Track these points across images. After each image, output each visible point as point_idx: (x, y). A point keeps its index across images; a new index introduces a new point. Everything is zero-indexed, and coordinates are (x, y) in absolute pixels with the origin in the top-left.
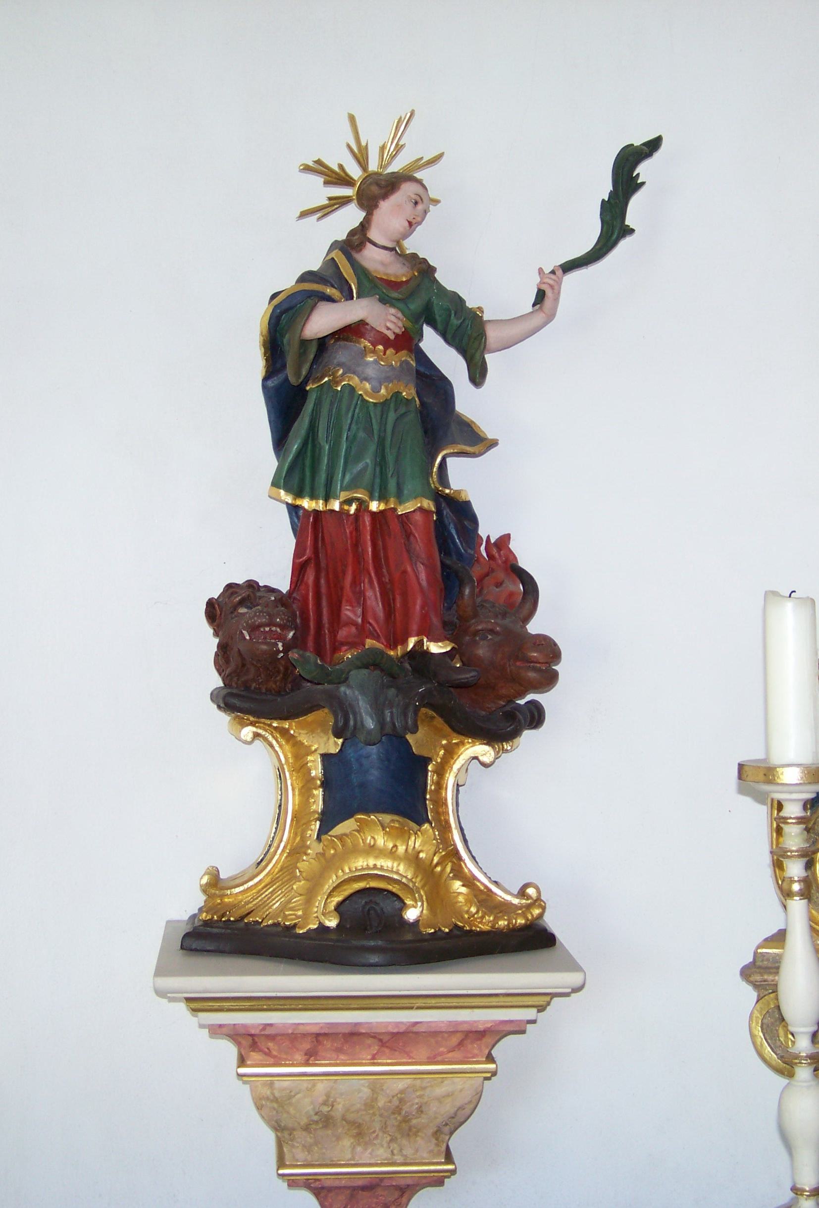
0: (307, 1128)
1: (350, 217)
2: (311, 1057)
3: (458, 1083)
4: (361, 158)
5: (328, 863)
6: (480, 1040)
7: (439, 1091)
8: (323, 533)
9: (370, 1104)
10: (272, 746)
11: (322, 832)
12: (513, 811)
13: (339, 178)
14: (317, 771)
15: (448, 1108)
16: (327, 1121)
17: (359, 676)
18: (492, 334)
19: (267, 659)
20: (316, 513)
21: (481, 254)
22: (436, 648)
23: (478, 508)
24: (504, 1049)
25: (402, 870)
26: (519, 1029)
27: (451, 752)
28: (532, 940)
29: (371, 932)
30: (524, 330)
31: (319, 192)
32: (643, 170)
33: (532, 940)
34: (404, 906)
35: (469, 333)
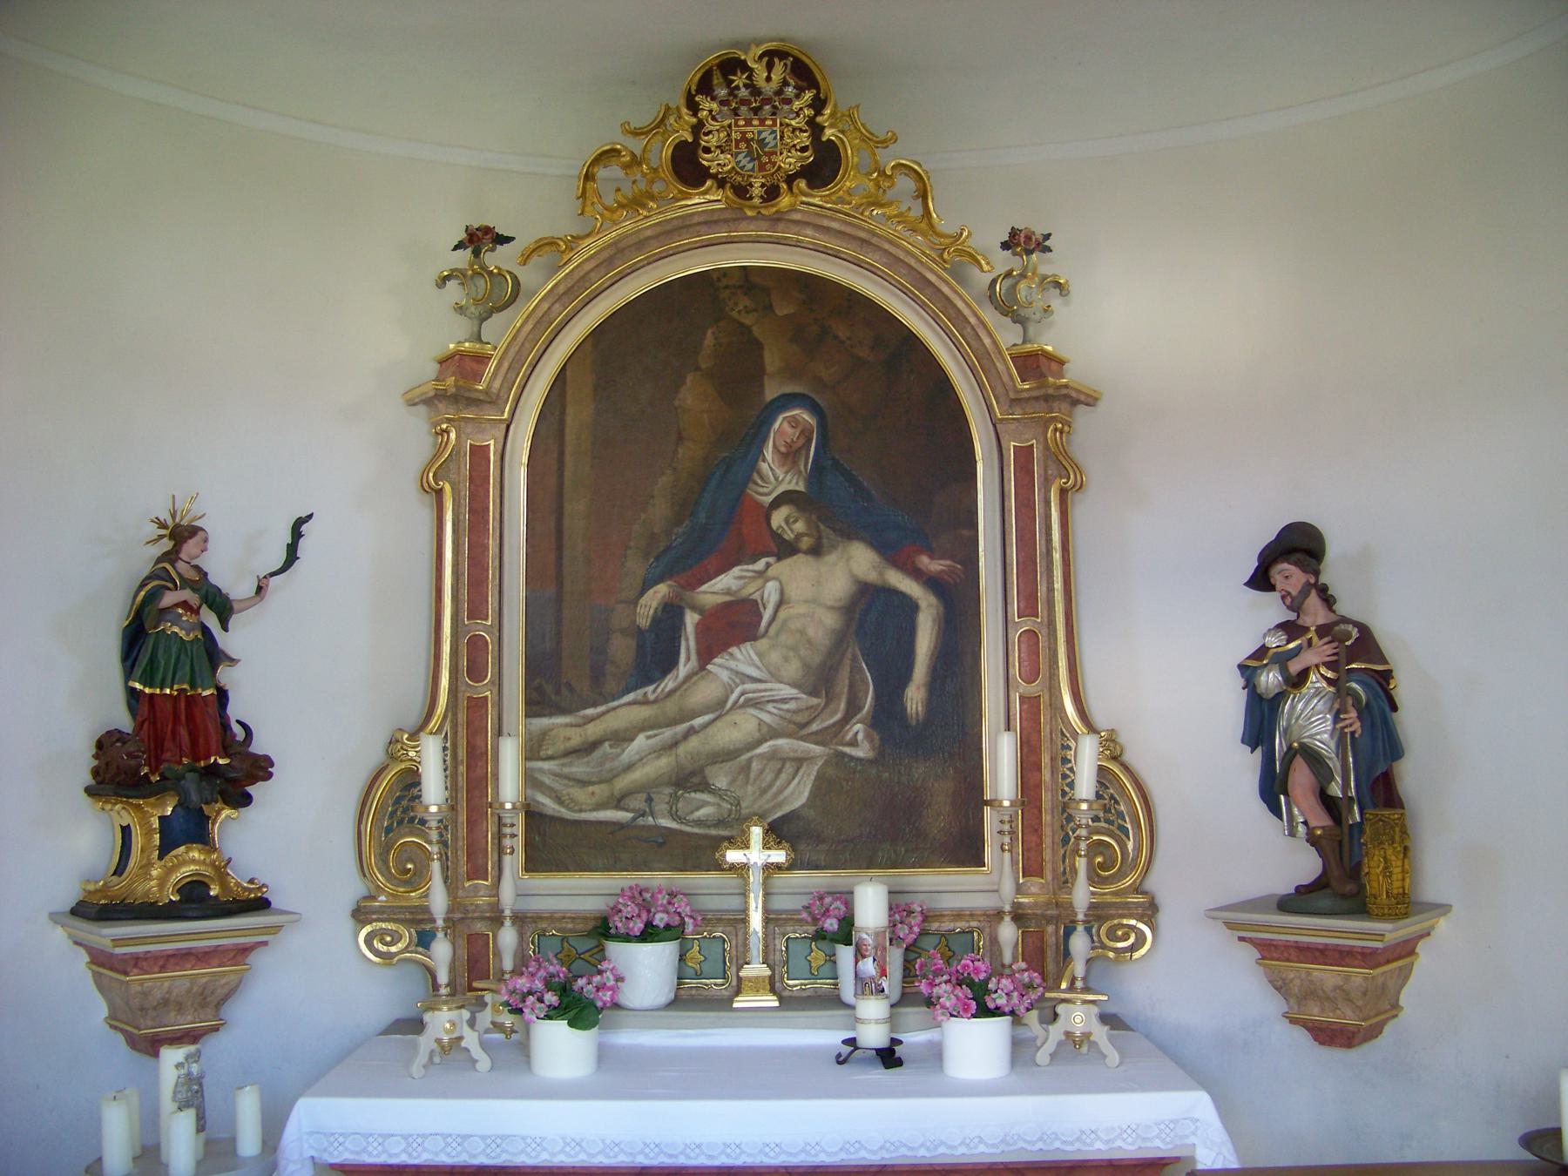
0: (155, 1008)
1: (167, 545)
2: (163, 969)
3: (233, 977)
4: (173, 516)
5: (169, 871)
6: (245, 951)
7: (223, 981)
8: (608, 711)
9: (189, 991)
10: (614, 709)
11: (161, 857)
12: (252, 840)
13: (163, 526)
14: (156, 825)
15: (225, 991)
16: (165, 1002)
17: (189, 776)
18: (236, 606)
19: (117, 773)
20: (152, 696)
21: (226, 566)
22: (221, 762)
23: (230, 695)
24: (256, 958)
25: (209, 871)
26: (265, 943)
27: (219, 813)
28: (261, 905)
29: (195, 900)
30: (248, 603)
31: (154, 531)
32: (304, 528)
33: (261, 905)
34: (209, 888)
35: (224, 608)
